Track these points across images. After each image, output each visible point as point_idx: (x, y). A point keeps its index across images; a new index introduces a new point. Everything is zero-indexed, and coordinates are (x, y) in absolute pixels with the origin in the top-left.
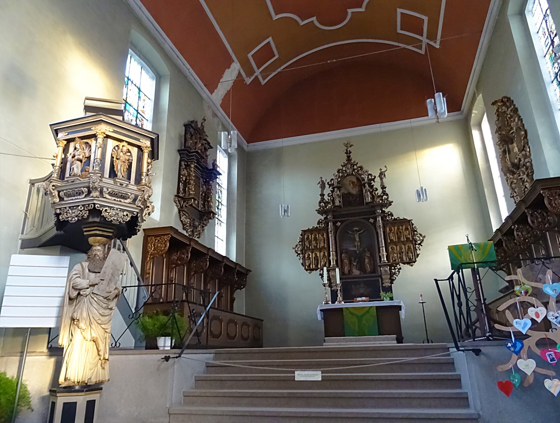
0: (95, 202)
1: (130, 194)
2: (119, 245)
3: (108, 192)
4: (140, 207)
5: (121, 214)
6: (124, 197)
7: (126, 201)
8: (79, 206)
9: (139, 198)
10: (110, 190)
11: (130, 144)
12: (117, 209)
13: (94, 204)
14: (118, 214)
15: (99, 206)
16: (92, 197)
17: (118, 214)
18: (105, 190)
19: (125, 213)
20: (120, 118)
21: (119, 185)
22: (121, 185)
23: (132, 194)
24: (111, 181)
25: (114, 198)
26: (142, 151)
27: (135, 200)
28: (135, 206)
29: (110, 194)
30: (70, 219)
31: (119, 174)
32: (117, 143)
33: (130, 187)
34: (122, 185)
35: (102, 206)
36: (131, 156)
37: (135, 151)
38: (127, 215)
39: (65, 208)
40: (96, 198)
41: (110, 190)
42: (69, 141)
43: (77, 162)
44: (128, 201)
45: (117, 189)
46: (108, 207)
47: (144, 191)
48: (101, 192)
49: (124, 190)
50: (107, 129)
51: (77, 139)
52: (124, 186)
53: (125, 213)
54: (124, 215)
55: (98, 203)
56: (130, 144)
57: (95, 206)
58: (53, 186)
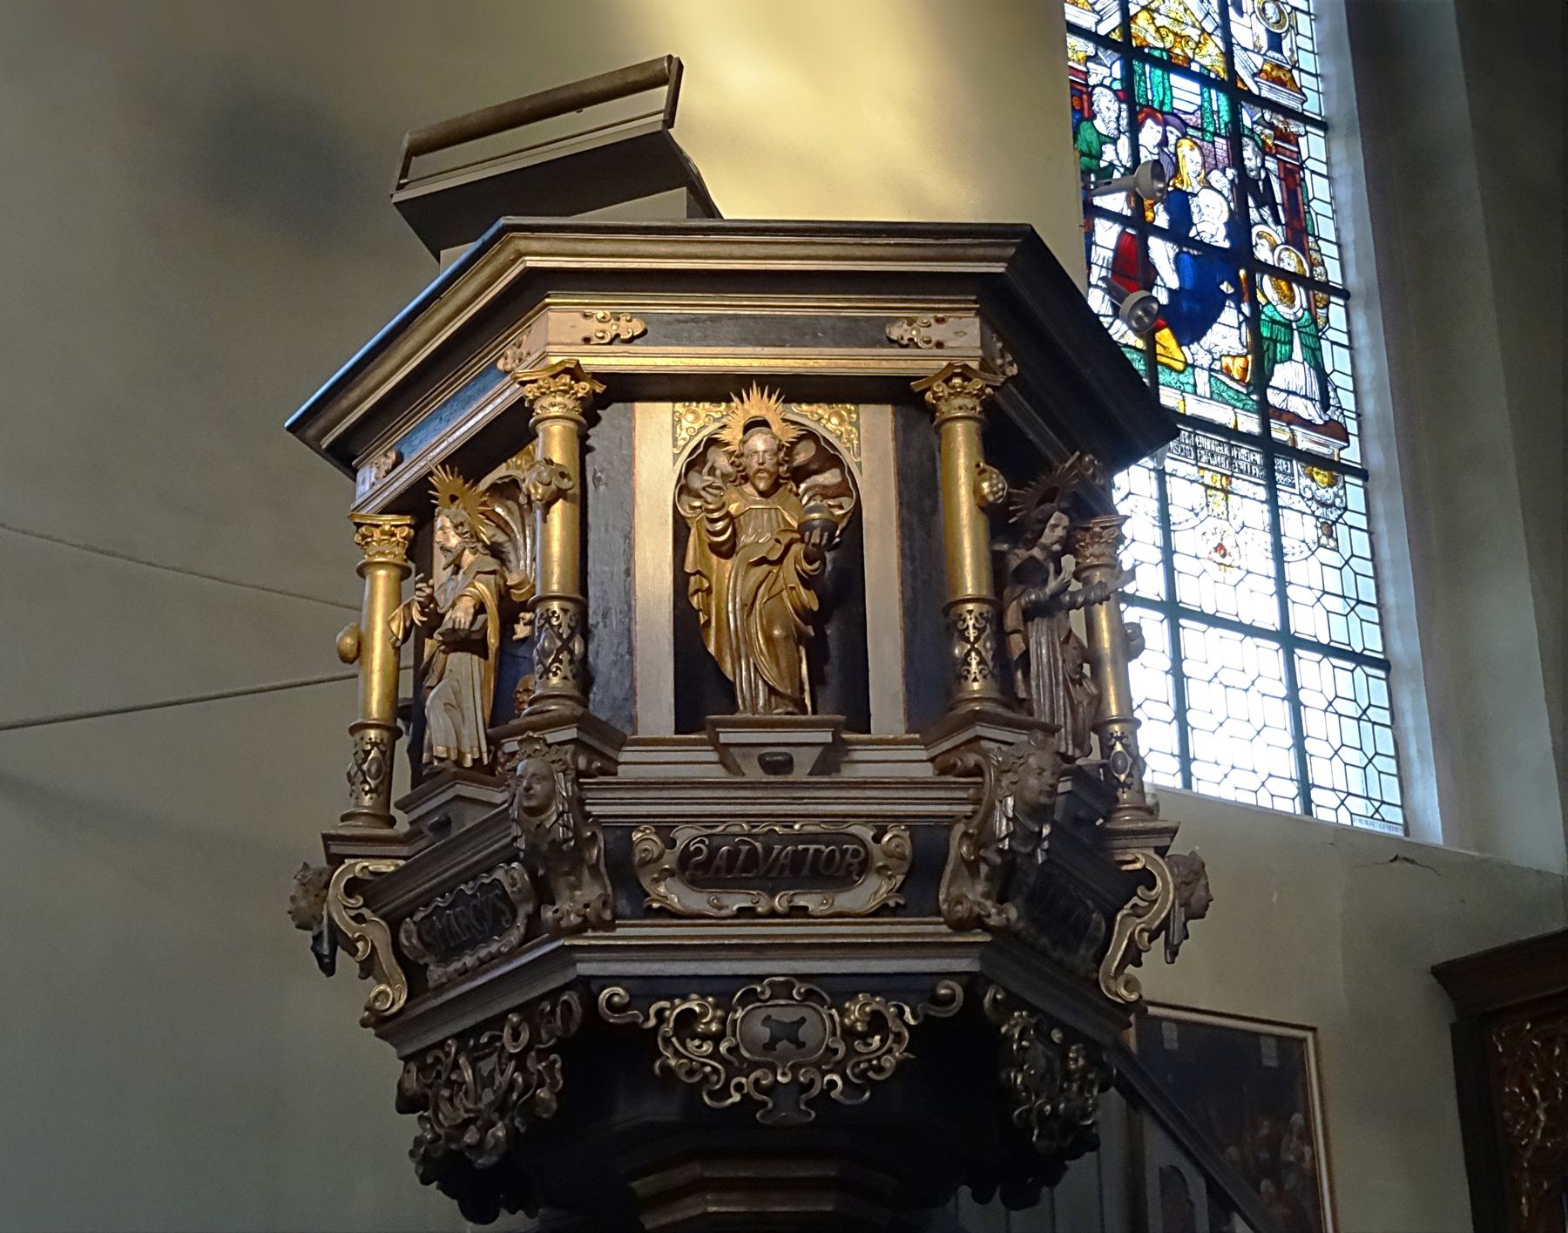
0: (584, 969)
1: (867, 834)
2: (1171, 1176)
3: (669, 860)
4: (979, 922)
5: (819, 1026)
6: (833, 866)
7: (845, 900)
8: (502, 1018)
9: (959, 849)
10: (683, 836)
11: (793, 388)
12: (783, 989)
13: (587, 987)
14: (791, 1032)
15: (619, 993)
16: (559, 932)
17: (791, 1032)
18: (645, 840)
19: (856, 1012)
20: (669, 205)
21: (754, 773)
22: (778, 765)
23: (880, 825)
24: (699, 762)
25: (736, 901)
26: (930, 411)
27: (922, 872)
28: (936, 929)
29: (701, 869)
30: (470, 1137)
31: (742, 677)
32: (698, 419)
33: (866, 763)
34: (786, 765)
35: (647, 989)
36: (847, 487)
37: (865, 438)
38: (877, 1023)
39: (441, 1044)
40: (590, 939)
41: (683, 836)
42: (417, 504)
43: (454, 657)
44: (870, 891)
45: (748, 812)
46: (702, 984)
47: (978, 771)
48: (623, 872)
49: (807, 811)
50: (592, 328)
51: (442, 479)
52: (800, 773)
53: (856, 1012)
54: (849, 1034)
55: (615, 961)
56: (793, 388)
57: (590, 1000)
58: (353, 887)
